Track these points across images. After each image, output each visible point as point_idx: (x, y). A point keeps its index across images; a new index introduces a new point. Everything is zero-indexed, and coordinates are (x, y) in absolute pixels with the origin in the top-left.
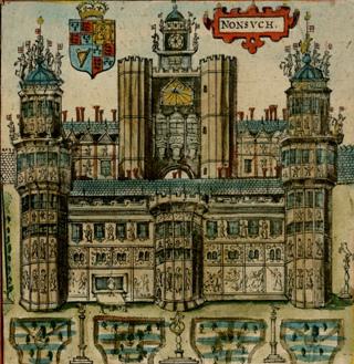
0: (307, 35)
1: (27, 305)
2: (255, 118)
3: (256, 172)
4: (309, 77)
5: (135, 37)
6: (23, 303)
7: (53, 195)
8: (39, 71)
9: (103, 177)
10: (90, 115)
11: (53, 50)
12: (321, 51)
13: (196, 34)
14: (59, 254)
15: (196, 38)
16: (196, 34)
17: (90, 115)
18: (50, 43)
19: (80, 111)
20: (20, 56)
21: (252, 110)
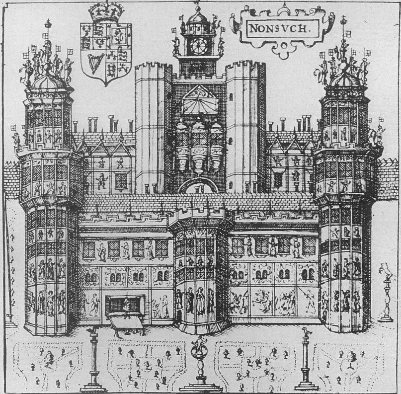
1: (33, 329)
6: (29, 327)
11: (63, 56)
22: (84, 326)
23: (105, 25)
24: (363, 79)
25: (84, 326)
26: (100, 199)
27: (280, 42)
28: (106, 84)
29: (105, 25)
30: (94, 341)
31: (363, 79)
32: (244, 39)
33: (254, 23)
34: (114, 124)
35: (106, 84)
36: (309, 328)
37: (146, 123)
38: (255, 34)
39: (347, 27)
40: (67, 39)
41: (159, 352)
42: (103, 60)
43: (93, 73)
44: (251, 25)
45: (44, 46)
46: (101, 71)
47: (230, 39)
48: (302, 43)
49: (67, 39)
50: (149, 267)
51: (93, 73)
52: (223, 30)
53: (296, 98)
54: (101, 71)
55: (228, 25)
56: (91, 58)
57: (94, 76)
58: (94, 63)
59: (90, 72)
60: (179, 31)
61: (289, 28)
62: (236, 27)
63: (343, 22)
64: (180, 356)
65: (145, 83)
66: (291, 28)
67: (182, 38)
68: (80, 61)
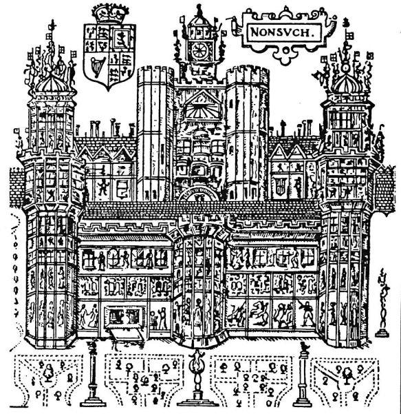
0: (346, 44)
1: (33, 342)
2: (287, 134)
3: (163, 289)
4: (347, 83)
5: (156, 48)
6: (30, 339)
7: (61, 217)
8: (49, 72)
9: (119, 200)
10: (105, 128)
11: (66, 58)
12: (362, 59)
13: (222, 42)
14: (36, 147)
15: (223, 45)
16: (222, 42)
17: (105, 128)
18: (62, 49)
19: (96, 124)
20: (30, 63)
21: (283, 124)
22: (82, 338)
23: (111, 26)
24: (50, 62)
25: (82, 338)
26: (94, 147)
27: (281, 46)
28: (108, 88)
29: (111, 26)
30: (93, 352)
31: (50, 62)
32: (246, 43)
33: (255, 27)
34: (115, 124)
35: (108, 88)
36: (307, 343)
37: (147, 128)
38: (255, 38)
39: (349, 30)
40: (70, 38)
41: (156, 366)
42: (105, 65)
43: (97, 77)
44: (252, 29)
45: (48, 47)
46: (103, 76)
47: (232, 43)
48: (250, 49)
49: (70, 38)
50: (148, 277)
51: (97, 77)
52: (224, 34)
53: (297, 99)
54: (103, 76)
55: (227, 26)
56: (94, 63)
57: (96, 80)
58: (97, 66)
59: (92, 75)
60: (180, 34)
61: (291, 32)
62: (236, 31)
63: (346, 24)
64: (177, 369)
65: (156, 87)
66: (294, 32)
67: (183, 41)
68: (83, 65)
